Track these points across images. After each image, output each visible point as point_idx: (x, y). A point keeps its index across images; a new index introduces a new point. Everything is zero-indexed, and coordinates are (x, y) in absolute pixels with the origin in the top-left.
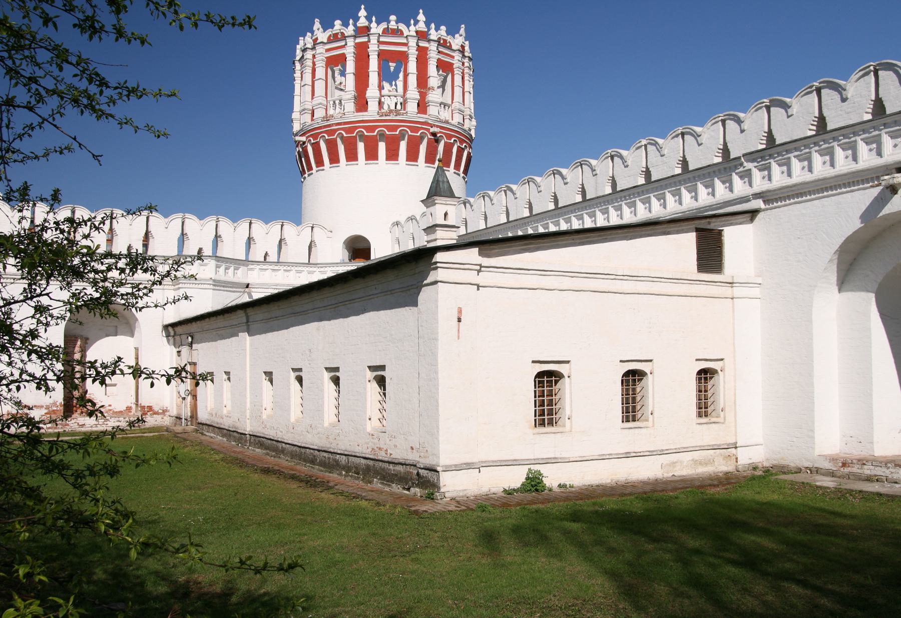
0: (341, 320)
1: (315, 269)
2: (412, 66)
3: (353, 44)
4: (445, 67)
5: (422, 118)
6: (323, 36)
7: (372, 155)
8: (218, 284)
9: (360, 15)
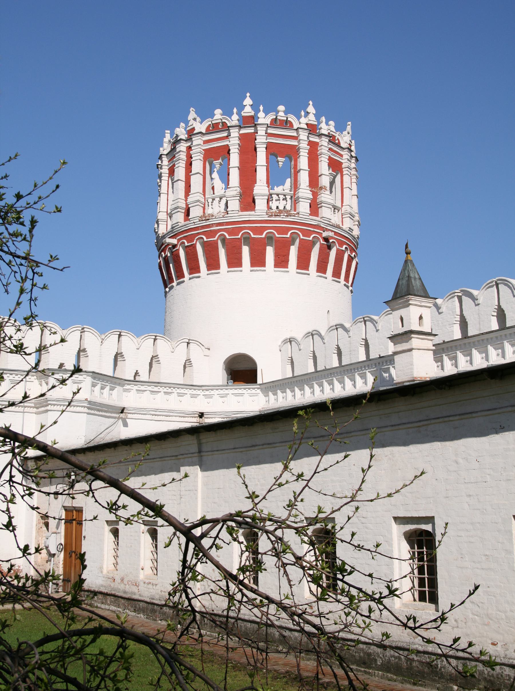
0: (437, 445)
1: (198, 392)
2: (303, 162)
3: (237, 135)
4: (335, 166)
5: (314, 220)
6: (200, 127)
7: (258, 261)
8: (95, 408)
9: (244, 104)
